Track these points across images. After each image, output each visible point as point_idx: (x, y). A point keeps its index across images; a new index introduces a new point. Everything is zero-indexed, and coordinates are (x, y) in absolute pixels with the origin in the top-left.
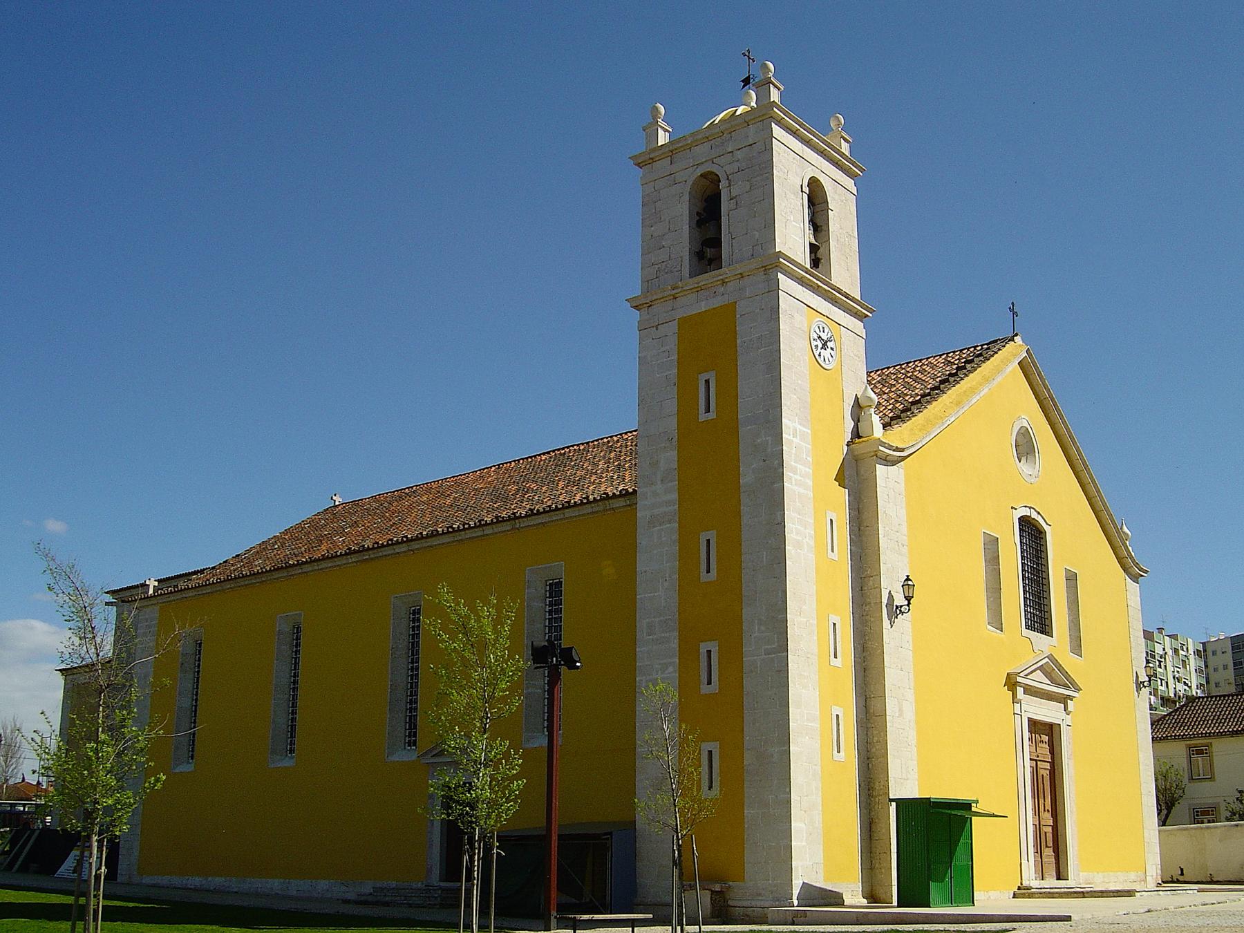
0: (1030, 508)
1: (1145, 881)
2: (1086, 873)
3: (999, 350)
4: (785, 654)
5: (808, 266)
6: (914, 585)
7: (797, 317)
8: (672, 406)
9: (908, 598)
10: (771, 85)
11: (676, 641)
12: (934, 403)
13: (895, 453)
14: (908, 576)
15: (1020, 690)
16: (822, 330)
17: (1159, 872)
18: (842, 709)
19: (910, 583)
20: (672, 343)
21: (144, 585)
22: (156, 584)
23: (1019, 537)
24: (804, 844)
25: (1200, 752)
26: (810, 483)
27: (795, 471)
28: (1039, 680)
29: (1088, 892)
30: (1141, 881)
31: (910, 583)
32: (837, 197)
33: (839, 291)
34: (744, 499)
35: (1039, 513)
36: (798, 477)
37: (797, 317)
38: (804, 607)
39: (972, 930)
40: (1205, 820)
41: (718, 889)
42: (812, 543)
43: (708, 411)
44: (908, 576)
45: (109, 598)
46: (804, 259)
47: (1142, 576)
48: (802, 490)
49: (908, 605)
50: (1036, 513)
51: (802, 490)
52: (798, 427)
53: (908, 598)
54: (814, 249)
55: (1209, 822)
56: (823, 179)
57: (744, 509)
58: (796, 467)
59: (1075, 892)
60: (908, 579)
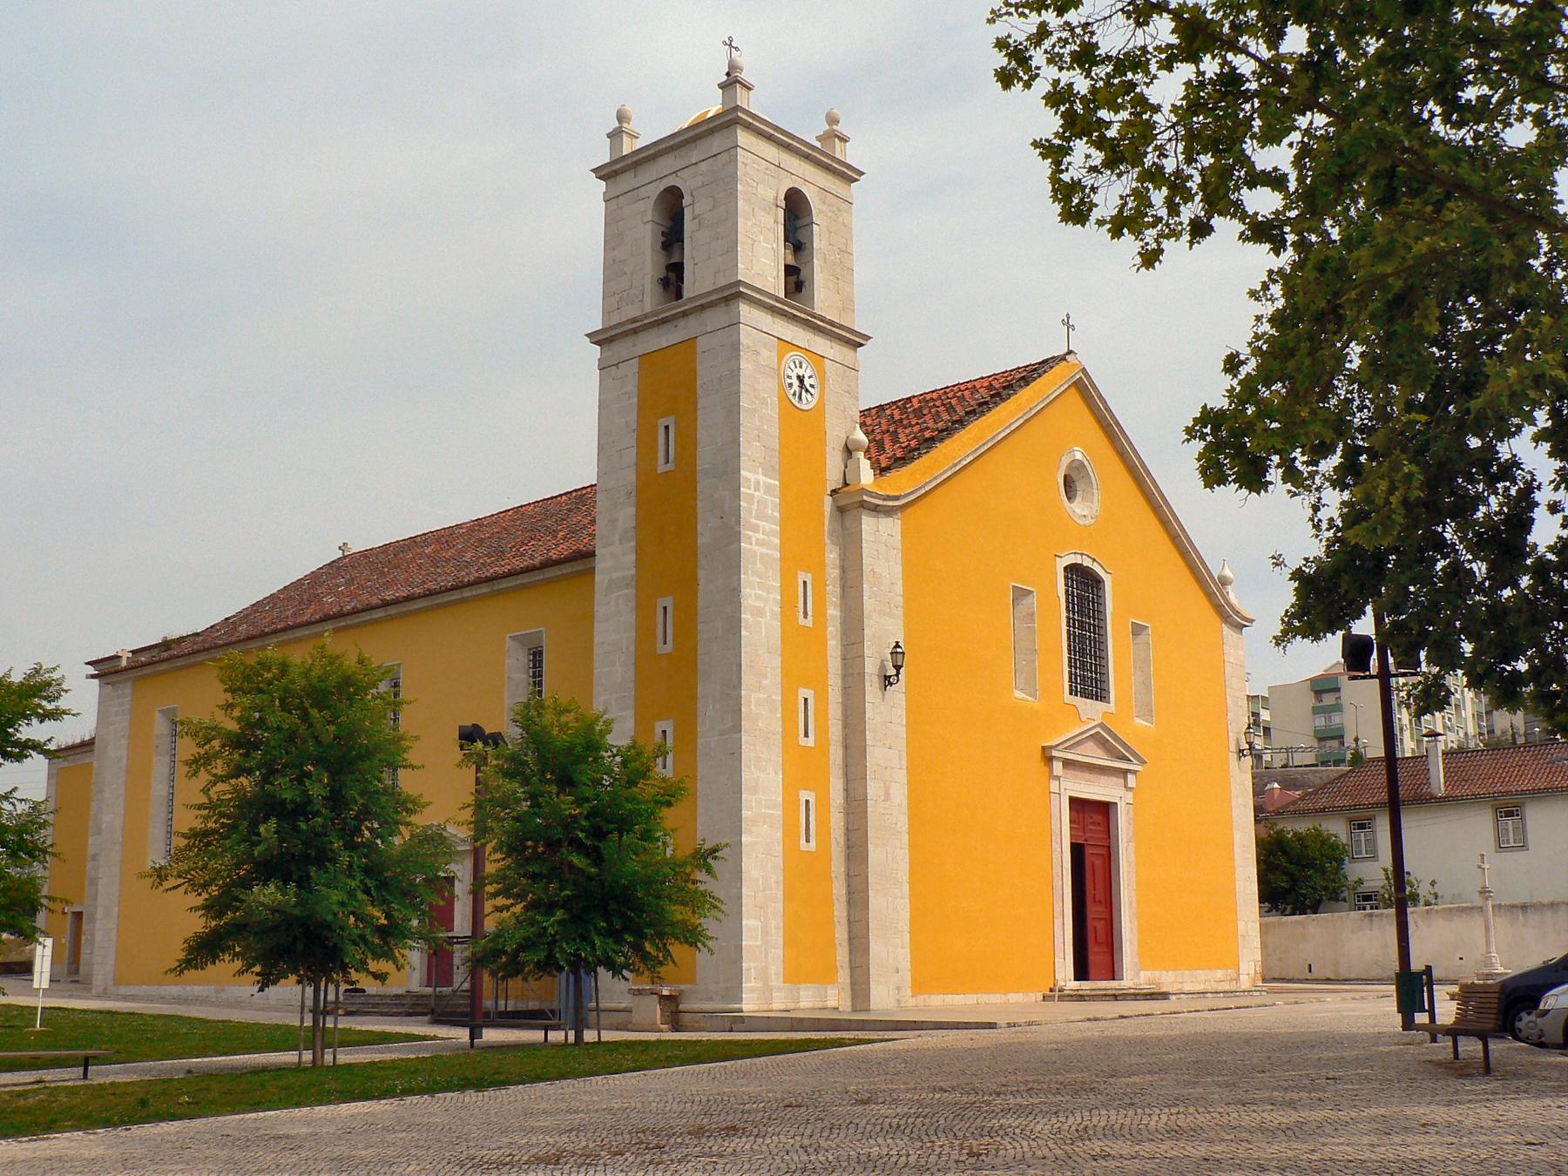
0: (1082, 554)
1: (1237, 980)
2: (1148, 973)
3: (1045, 372)
4: (738, 735)
5: (782, 295)
6: (903, 653)
7: (764, 352)
8: (631, 456)
9: (898, 668)
10: (738, 85)
11: (632, 721)
12: (947, 442)
13: (885, 503)
14: (897, 643)
15: (1058, 767)
16: (798, 365)
17: (1259, 969)
18: (813, 794)
19: (899, 650)
20: (632, 385)
21: (116, 657)
22: (130, 655)
23: (1064, 588)
24: (759, 943)
25: (1362, 827)
26: (777, 541)
27: (755, 529)
28: (1092, 754)
29: (1119, 995)
30: (1231, 980)
31: (899, 650)
32: (824, 208)
33: (822, 319)
34: (702, 562)
35: (1094, 560)
36: (761, 536)
37: (764, 352)
38: (764, 682)
39: (1371, 1030)
40: (1368, 907)
41: (665, 993)
42: (777, 609)
43: (667, 462)
44: (897, 643)
45: (91, 670)
46: (774, 282)
47: (1246, 626)
48: (765, 551)
49: (897, 675)
50: (1090, 560)
51: (765, 551)
52: (762, 478)
53: (898, 668)
54: (790, 271)
55: (1372, 908)
56: (810, 193)
57: (701, 573)
58: (757, 525)
59: (1106, 995)
60: (897, 646)
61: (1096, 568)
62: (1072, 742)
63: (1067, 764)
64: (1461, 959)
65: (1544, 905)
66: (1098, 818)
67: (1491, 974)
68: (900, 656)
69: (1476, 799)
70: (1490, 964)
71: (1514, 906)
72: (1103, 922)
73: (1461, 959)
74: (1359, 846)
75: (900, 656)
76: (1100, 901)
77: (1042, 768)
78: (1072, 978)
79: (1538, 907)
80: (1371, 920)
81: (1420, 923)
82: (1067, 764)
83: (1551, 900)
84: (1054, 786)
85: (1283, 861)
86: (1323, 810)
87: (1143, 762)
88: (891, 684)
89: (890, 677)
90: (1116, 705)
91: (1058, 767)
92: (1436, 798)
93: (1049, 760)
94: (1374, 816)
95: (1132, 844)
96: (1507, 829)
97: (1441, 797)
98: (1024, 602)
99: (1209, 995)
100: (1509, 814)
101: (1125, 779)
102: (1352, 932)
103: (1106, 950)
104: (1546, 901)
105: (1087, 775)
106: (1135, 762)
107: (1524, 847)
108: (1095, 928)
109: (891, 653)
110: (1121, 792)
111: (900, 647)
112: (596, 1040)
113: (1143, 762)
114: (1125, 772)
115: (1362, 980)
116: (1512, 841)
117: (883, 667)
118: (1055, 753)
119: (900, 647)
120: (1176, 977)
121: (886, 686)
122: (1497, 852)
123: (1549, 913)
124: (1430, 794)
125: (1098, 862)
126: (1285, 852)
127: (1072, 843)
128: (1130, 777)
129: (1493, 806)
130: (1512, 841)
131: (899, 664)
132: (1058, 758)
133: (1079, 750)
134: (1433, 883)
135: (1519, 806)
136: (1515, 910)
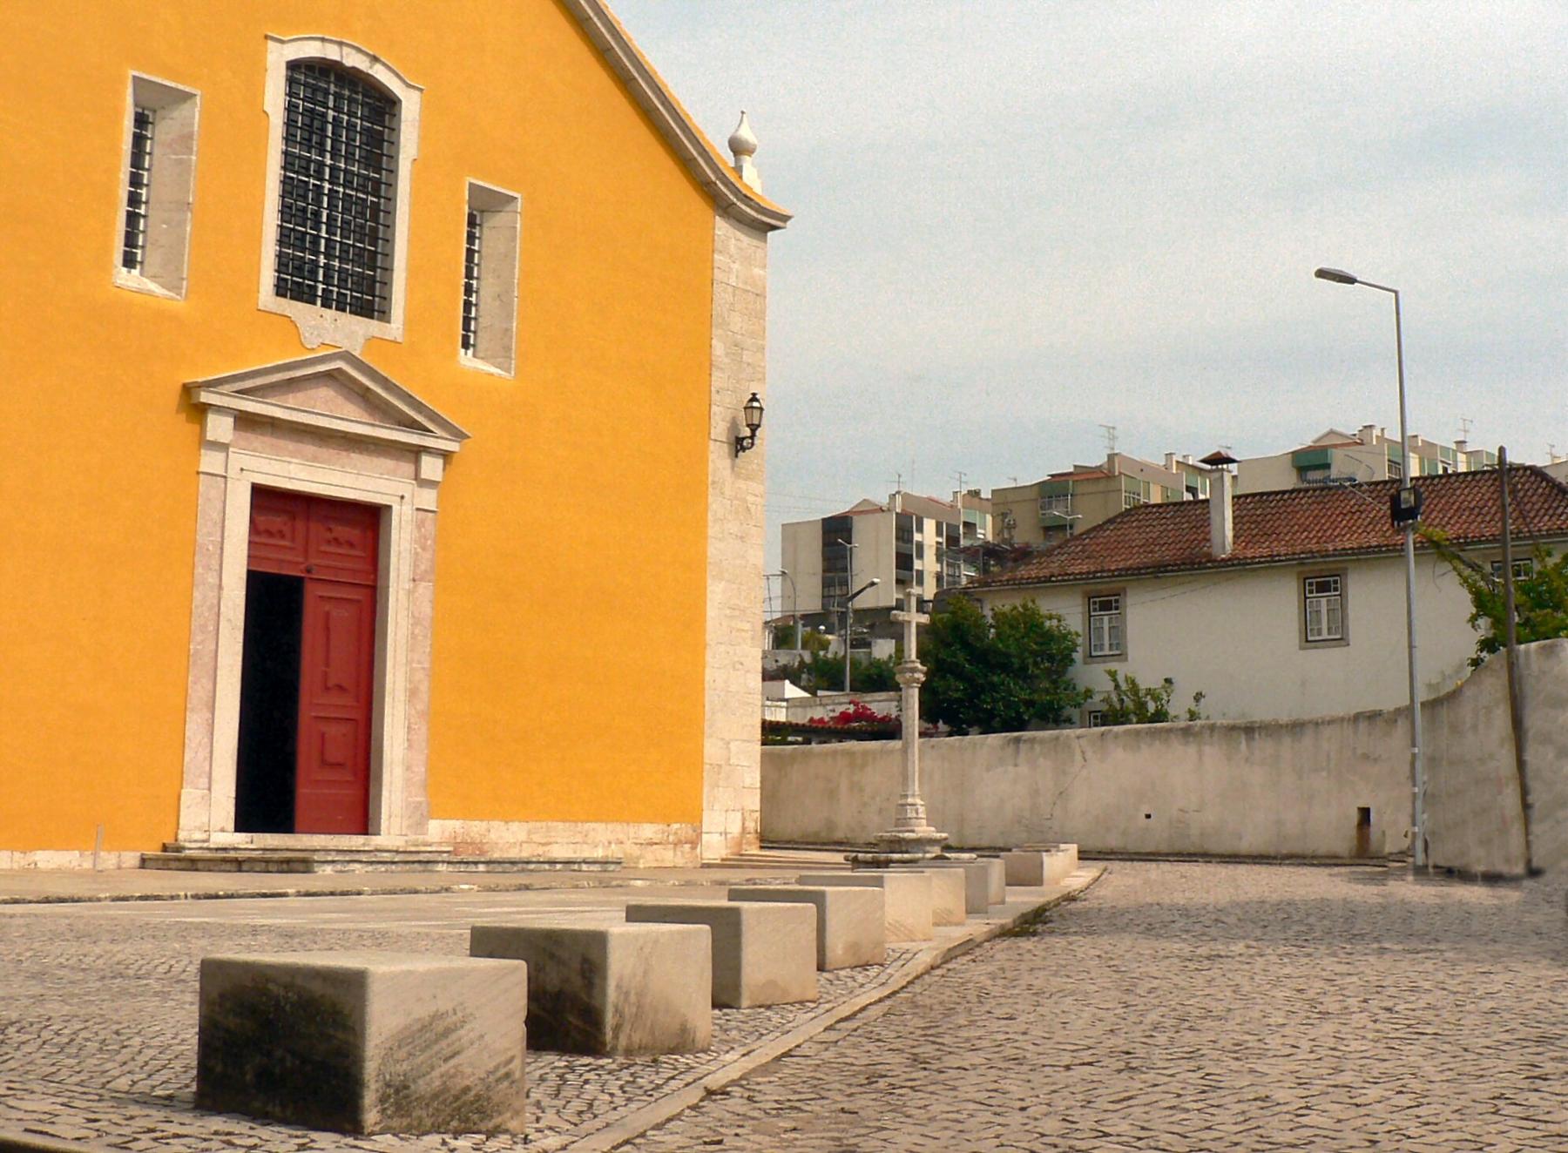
14: (754, 394)
15: (220, 427)
25: (1106, 606)
31: (755, 404)
49: (752, 437)
53: (754, 428)
61: (380, 74)
62: (259, 381)
63: (246, 421)
64: (1148, 816)
65: (1281, 726)
66: (354, 533)
67: (900, 841)
68: (756, 413)
69: (1271, 565)
70: (903, 822)
71: (1233, 728)
72: (343, 729)
73: (1148, 816)
74: (1101, 638)
75: (756, 413)
76: (340, 688)
77: (184, 428)
78: (231, 826)
79: (1271, 729)
80: (1017, 751)
81: (1089, 755)
82: (246, 421)
83: (1294, 717)
84: (210, 461)
85: (961, 657)
86: (1048, 579)
87: (459, 435)
88: (744, 449)
89: (744, 439)
90: (409, 323)
91: (220, 427)
92: (1215, 561)
93: (199, 411)
94: (1124, 589)
95: (425, 589)
96: (1318, 612)
97: (1223, 560)
98: (176, 114)
99: (559, 866)
100: (1323, 587)
101: (417, 462)
102: (988, 770)
103: (350, 778)
104: (1284, 719)
105: (310, 449)
106: (439, 432)
107: (1343, 641)
108: (323, 736)
109: (745, 408)
110: (407, 487)
111: (757, 400)
112: (991, 901)
113: (459, 435)
114: (416, 452)
115: (808, 843)
116: (1325, 631)
117: (734, 425)
118: (205, 397)
119: (757, 400)
120: (529, 832)
121: (737, 452)
122: (1301, 648)
123: (1287, 741)
124: (1209, 554)
125: (341, 614)
126: (966, 645)
127: (249, 572)
128: (426, 460)
129: (1299, 573)
130: (1325, 631)
131: (756, 422)
132: (220, 410)
133: (292, 399)
134: (1198, 697)
135: (1340, 574)
136: (1235, 734)
